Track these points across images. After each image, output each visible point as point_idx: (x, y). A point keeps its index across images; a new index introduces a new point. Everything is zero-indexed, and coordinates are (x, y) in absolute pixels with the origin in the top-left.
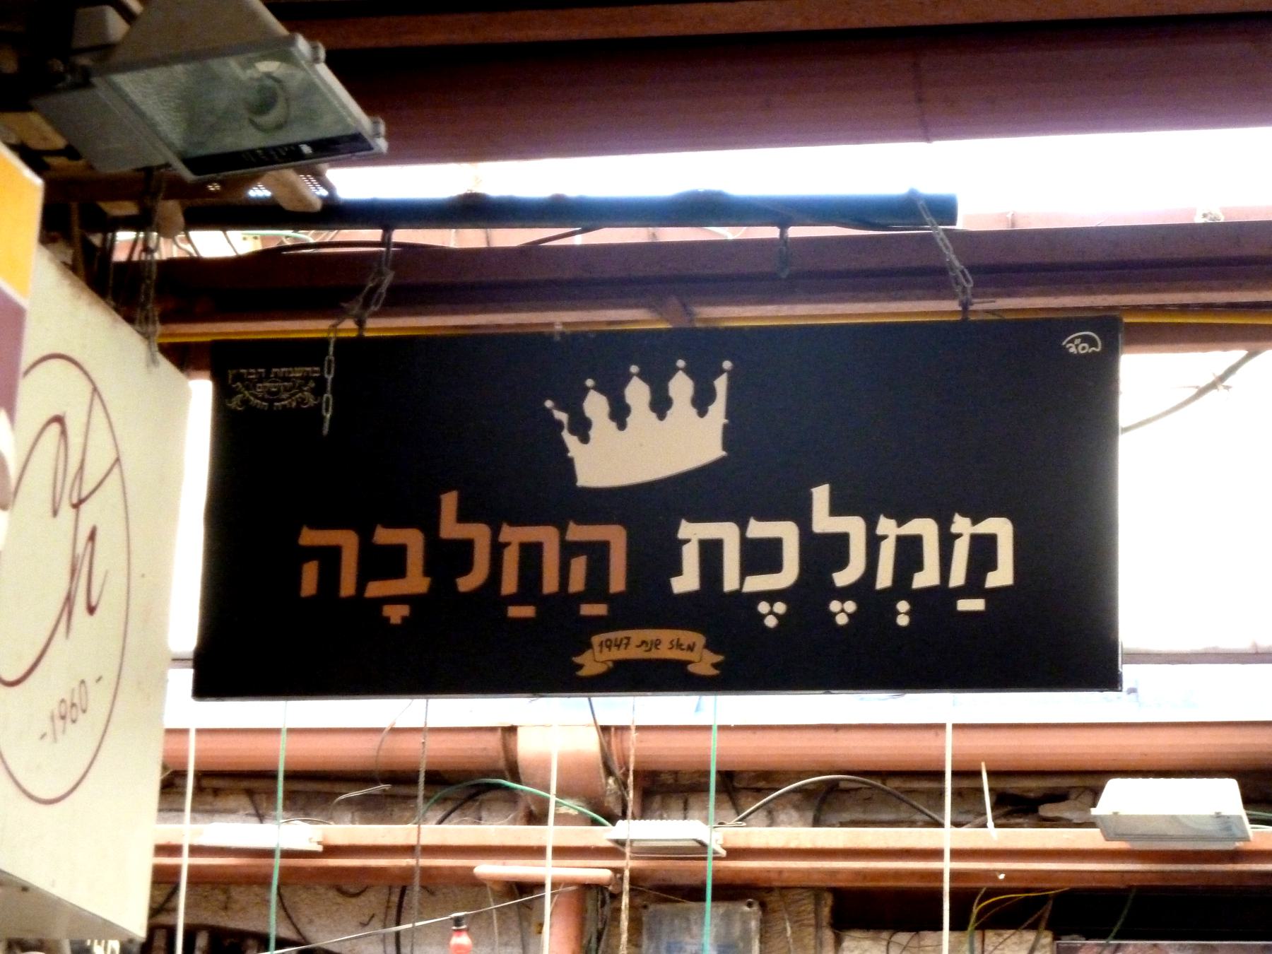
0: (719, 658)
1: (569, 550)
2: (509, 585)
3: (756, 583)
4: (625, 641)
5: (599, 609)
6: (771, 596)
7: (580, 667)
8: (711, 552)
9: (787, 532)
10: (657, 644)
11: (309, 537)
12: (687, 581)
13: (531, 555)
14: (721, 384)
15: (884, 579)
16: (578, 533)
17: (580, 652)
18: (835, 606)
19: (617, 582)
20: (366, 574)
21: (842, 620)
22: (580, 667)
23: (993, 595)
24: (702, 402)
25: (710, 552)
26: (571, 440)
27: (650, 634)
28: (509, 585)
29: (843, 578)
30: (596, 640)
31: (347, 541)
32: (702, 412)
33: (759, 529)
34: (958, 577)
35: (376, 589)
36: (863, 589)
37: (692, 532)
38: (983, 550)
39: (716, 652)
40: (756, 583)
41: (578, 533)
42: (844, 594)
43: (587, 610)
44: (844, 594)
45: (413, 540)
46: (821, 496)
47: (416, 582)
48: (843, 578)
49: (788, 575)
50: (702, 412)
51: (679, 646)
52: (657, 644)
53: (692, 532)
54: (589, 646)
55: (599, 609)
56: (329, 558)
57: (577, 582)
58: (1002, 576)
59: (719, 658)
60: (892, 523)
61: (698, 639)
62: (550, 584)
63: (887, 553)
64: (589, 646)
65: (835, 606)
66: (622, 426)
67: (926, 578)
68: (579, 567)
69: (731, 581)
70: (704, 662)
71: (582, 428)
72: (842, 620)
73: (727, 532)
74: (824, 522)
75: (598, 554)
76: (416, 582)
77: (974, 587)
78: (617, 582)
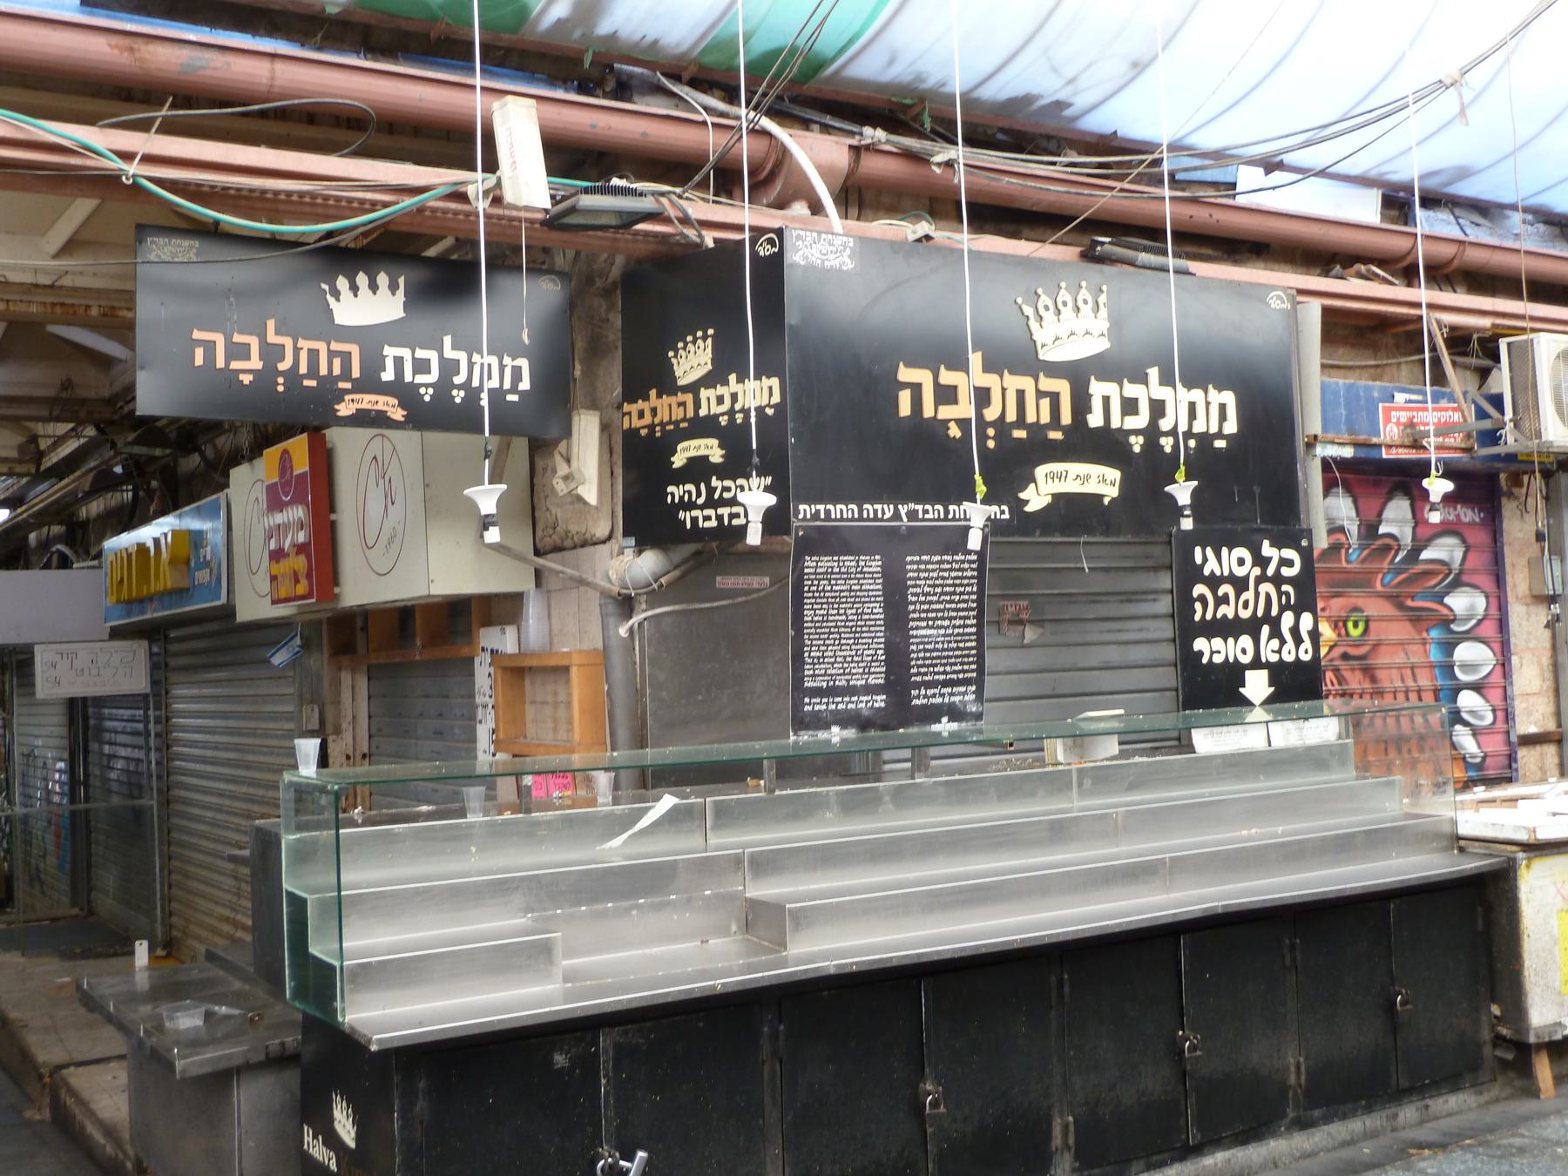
0: (405, 413)
1: (332, 354)
2: (303, 369)
3: (420, 379)
4: (1064, 474)
5: (348, 385)
6: (427, 386)
7: (1026, 502)
8: (399, 362)
9: (432, 356)
10: (1088, 477)
11: (197, 335)
12: (388, 375)
13: (313, 355)
14: (401, 281)
15: (476, 383)
16: (335, 346)
17: (338, 403)
18: (455, 392)
19: (356, 373)
20: (229, 358)
21: (458, 400)
22: (1026, 502)
23: (522, 394)
24: (393, 288)
25: (399, 362)
26: (1033, 324)
27: (374, 398)
28: (303, 369)
29: (458, 380)
30: (1041, 471)
31: (219, 339)
32: (394, 294)
33: (421, 354)
34: (507, 385)
35: (235, 365)
36: (466, 386)
37: (390, 352)
38: (517, 372)
39: (722, 449)
40: (420, 379)
41: (335, 346)
42: (459, 387)
43: (342, 385)
44: (459, 387)
45: (254, 342)
46: (447, 340)
47: (255, 363)
48: (458, 380)
49: (433, 377)
50: (394, 294)
51: (388, 405)
52: (1088, 477)
53: (390, 352)
54: (344, 400)
55: (348, 385)
56: (210, 347)
57: (337, 371)
58: (525, 385)
59: (405, 413)
60: (510, 359)
61: (395, 401)
62: (323, 371)
63: (508, 372)
64: (344, 400)
65: (455, 392)
66: (356, 296)
67: (1199, 427)
68: (337, 362)
69: (928, 411)
70: (398, 414)
71: (336, 294)
72: (458, 400)
73: (405, 353)
74: (449, 353)
75: (1055, 398)
76: (255, 363)
77: (514, 390)
78: (356, 373)
